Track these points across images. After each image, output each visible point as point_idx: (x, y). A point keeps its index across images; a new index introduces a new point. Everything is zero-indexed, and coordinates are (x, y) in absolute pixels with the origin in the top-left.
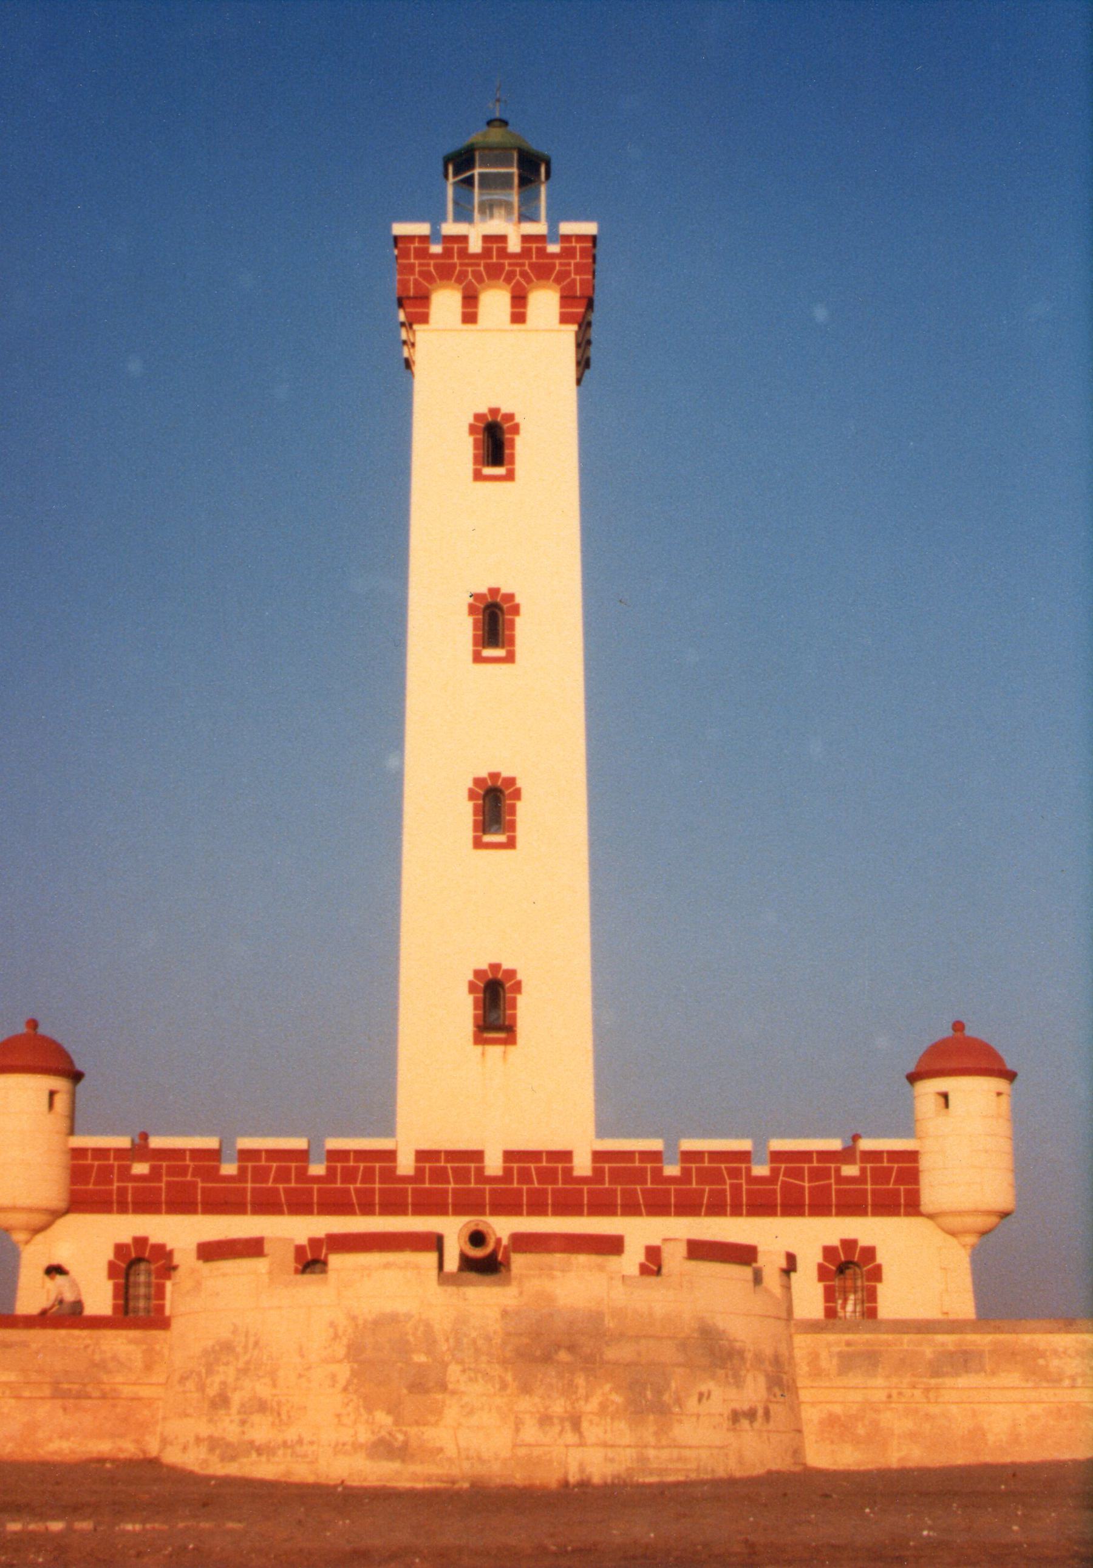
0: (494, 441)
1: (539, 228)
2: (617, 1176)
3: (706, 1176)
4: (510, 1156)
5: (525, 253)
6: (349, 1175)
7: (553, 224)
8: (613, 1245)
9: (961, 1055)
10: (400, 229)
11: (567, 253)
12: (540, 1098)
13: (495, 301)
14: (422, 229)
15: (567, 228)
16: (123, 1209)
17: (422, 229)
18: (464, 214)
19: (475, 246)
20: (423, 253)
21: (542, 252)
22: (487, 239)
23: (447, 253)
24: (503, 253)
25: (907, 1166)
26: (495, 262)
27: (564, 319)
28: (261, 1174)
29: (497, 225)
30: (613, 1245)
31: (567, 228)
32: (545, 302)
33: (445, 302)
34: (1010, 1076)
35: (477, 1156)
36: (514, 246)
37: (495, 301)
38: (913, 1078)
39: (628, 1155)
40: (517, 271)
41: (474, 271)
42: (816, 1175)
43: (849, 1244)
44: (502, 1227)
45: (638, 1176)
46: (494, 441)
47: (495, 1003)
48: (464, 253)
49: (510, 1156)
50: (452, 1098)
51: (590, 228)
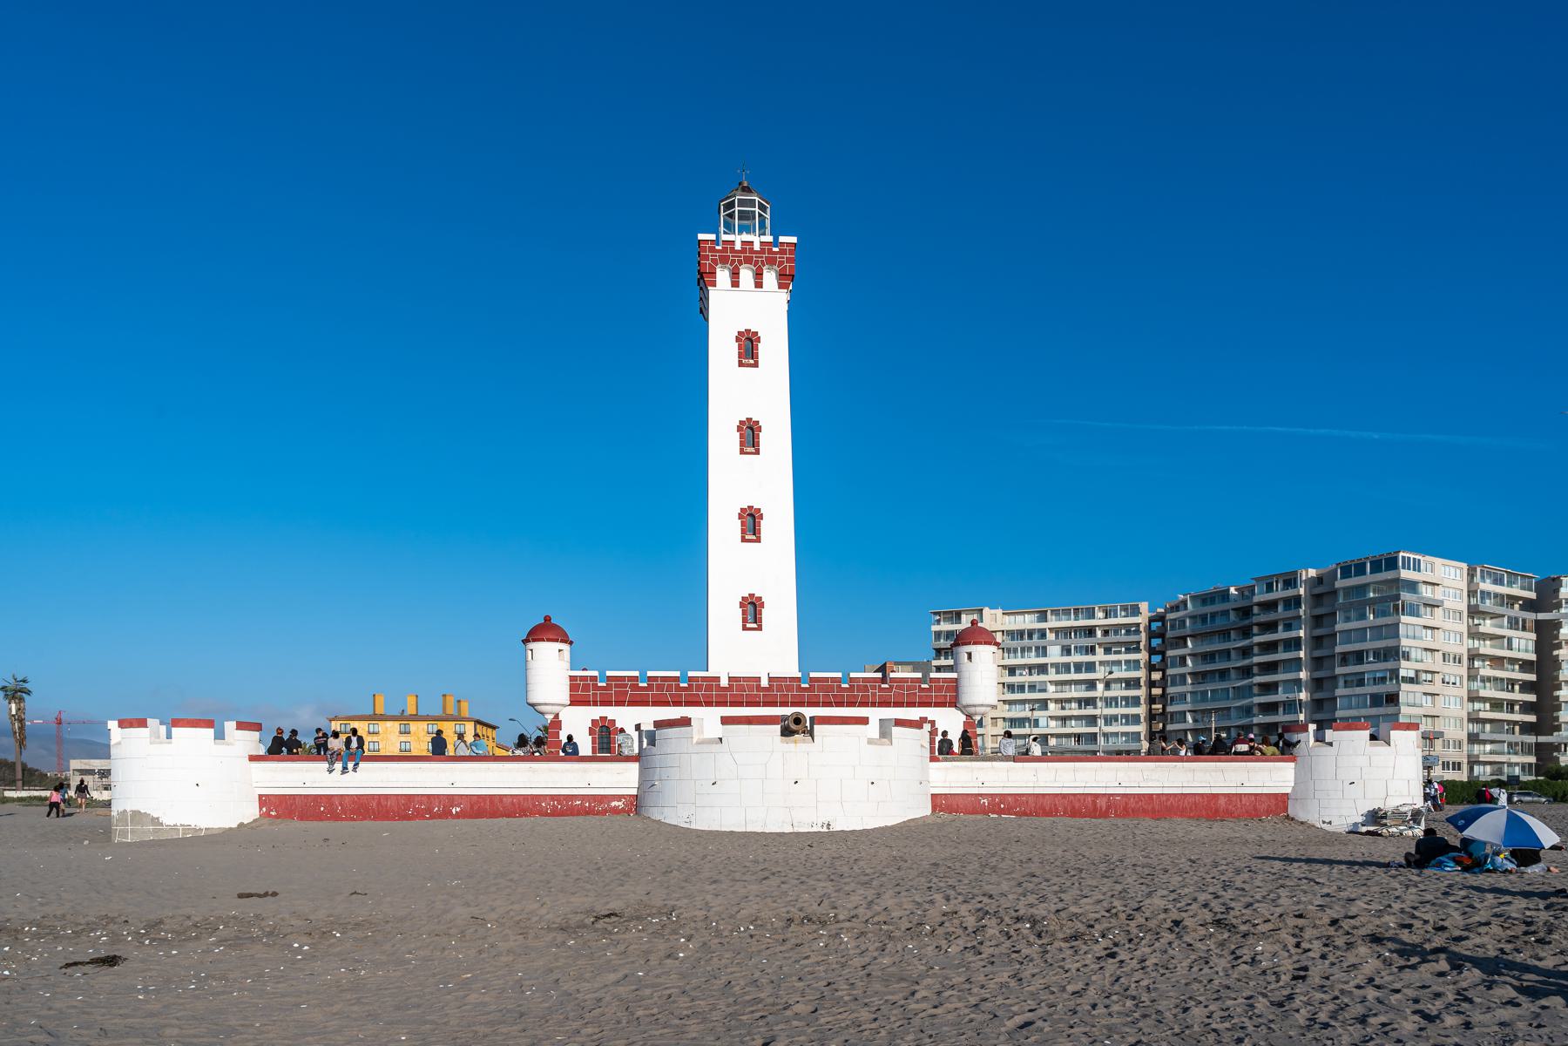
0: (748, 346)
1: (769, 238)
2: (780, 689)
3: (659, 688)
4: (771, 679)
5: (762, 251)
6: (699, 688)
7: (776, 239)
8: (864, 721)
9: (545, 631)
10: (701, 236)
11: (782, 252)
12: (773, 653)
13: (746, 275)
14: (712, 237)
15: (782, 239)
16: (595, 704)
17: (712, 237)
18: (729, 228)
19: (738, 247)
20: (713, 250)
21: (770, 251)
22: (743, 243)
23: (725, 249)
24: (752, 251)
25: (955, 686)
26: (748, 255)
27: (781, 286)
28: (659, 688)
29: (746, 237)
30: (864, 721)
31: (782, 239)
32: (770, 277)
33: (723, 276)
34: (566, 640)
35: (718, 679)
36: (757, 247)
37: (746, 275)
38: (525, 641)
39: (623, 678)
40: (757, 260)
41: (735, 259)
42: (909, 688)
43: (603, 719)
44: (808, 712)
45: (830, 689)
46: (748, 346)
47: (752, 609)
48: (733, 250)
49: (771, 679)
50: (733, 653)
51: (794, 240)
